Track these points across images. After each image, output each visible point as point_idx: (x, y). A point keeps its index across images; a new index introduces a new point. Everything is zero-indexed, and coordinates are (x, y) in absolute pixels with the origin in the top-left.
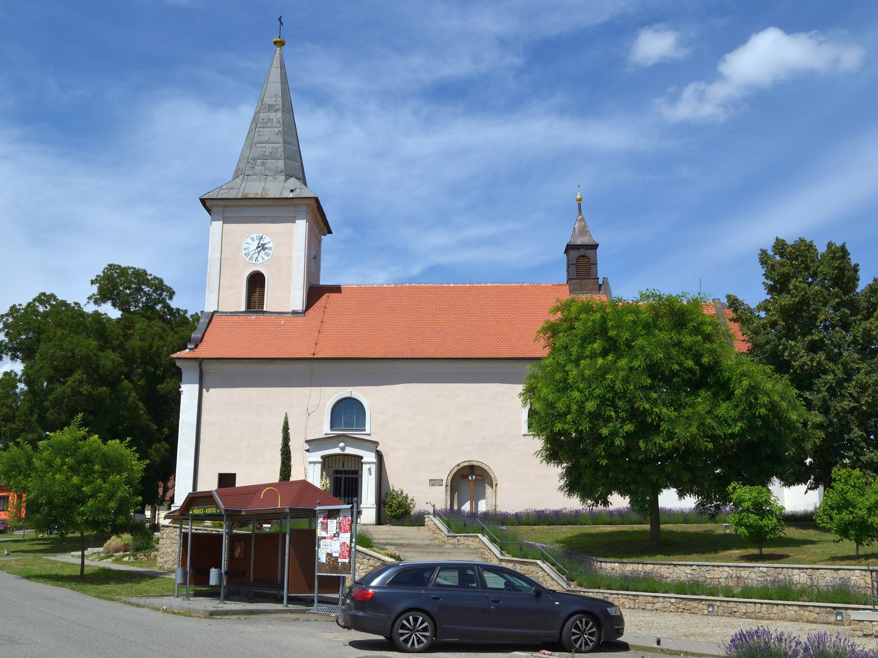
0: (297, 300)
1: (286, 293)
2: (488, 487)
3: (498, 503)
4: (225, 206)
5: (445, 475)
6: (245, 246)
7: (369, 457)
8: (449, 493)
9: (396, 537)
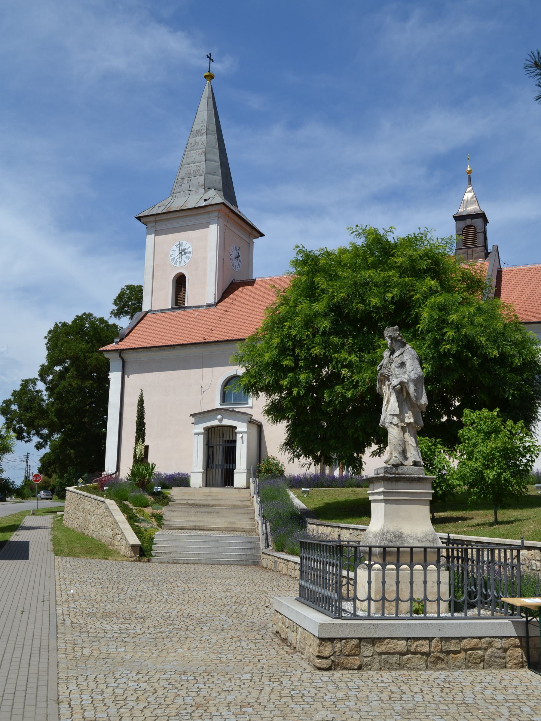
1: (203, 289)
4: (156, 222)
6: (171, 253)
7: (242, 427)
9: (210, 498)
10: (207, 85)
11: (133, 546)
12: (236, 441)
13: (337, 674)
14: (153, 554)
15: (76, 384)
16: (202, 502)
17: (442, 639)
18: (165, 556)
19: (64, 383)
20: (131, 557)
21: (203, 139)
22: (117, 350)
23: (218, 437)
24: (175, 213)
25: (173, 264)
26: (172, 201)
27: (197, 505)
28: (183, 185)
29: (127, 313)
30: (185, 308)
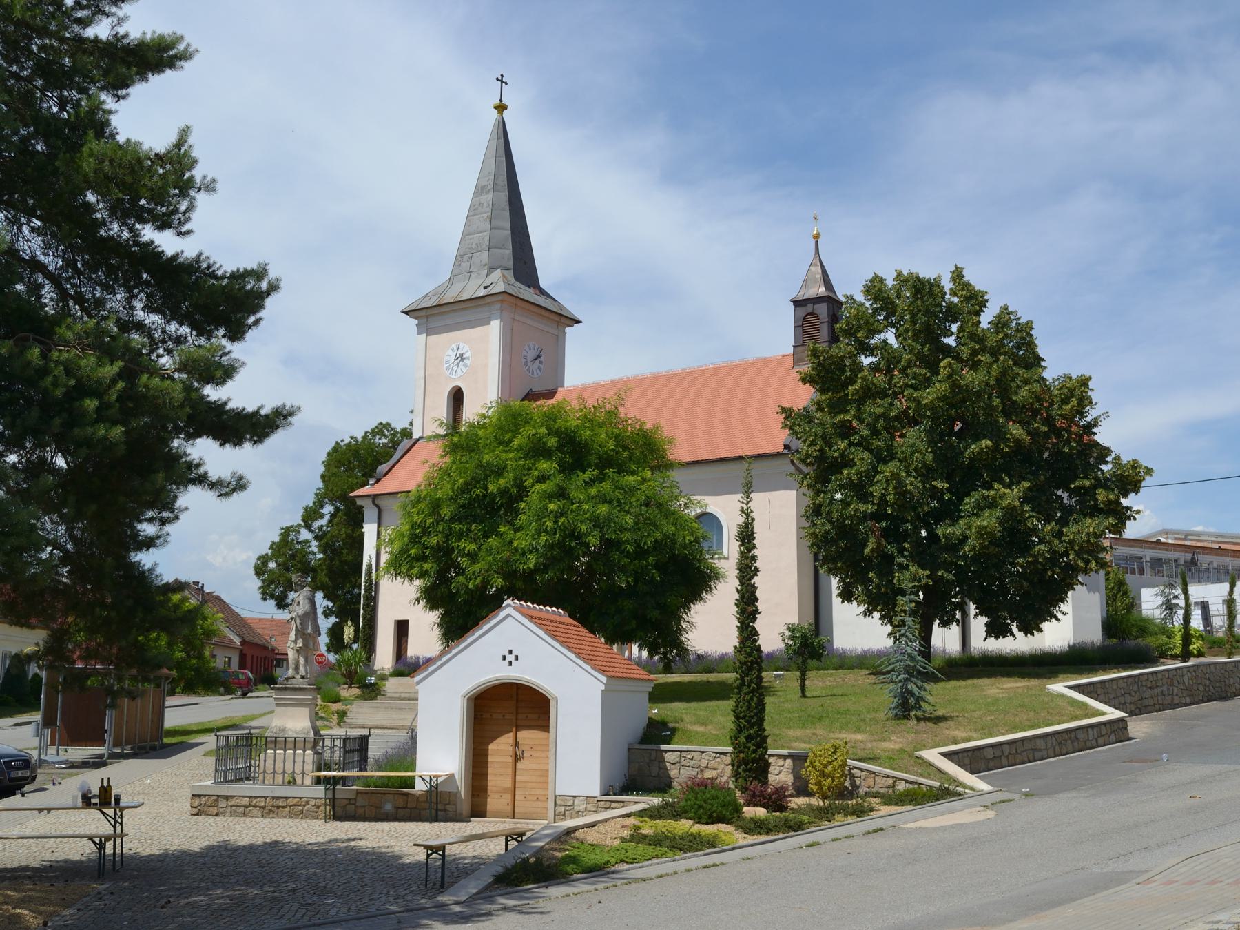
4: (427, 317)
6: (447, 358)
13: (200, 818)
17: (273, 798)
22: (368, 496)
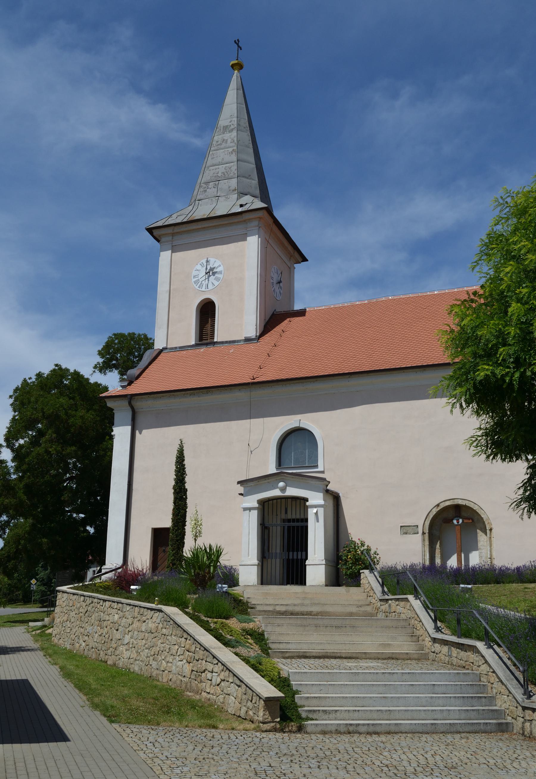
0: (250, 326)
1: (239, 319)
2: (480, 533)
3: (494, 555)
4: (173, 235)
5: (420, 518)
6: (194, 273)
7: (316, 499)
8: (427, 543)
9: (307, 602)
10: (235, 74)
11: (269, 701)
12: (307, 519)
14: (304, 715)
15: (55, 449)
16: (297, 609)
18: (326, 716)
19: (39, 450)
20: (264, 723)
21: (232, 137)
22: (125, 396)
23: (275, 514)
24: (199, 223)
25: (197, 287)
26: (194, 209)
27: (292, 614)
28: (208, 190)
29: (116, 367)
30: (214, 343)
